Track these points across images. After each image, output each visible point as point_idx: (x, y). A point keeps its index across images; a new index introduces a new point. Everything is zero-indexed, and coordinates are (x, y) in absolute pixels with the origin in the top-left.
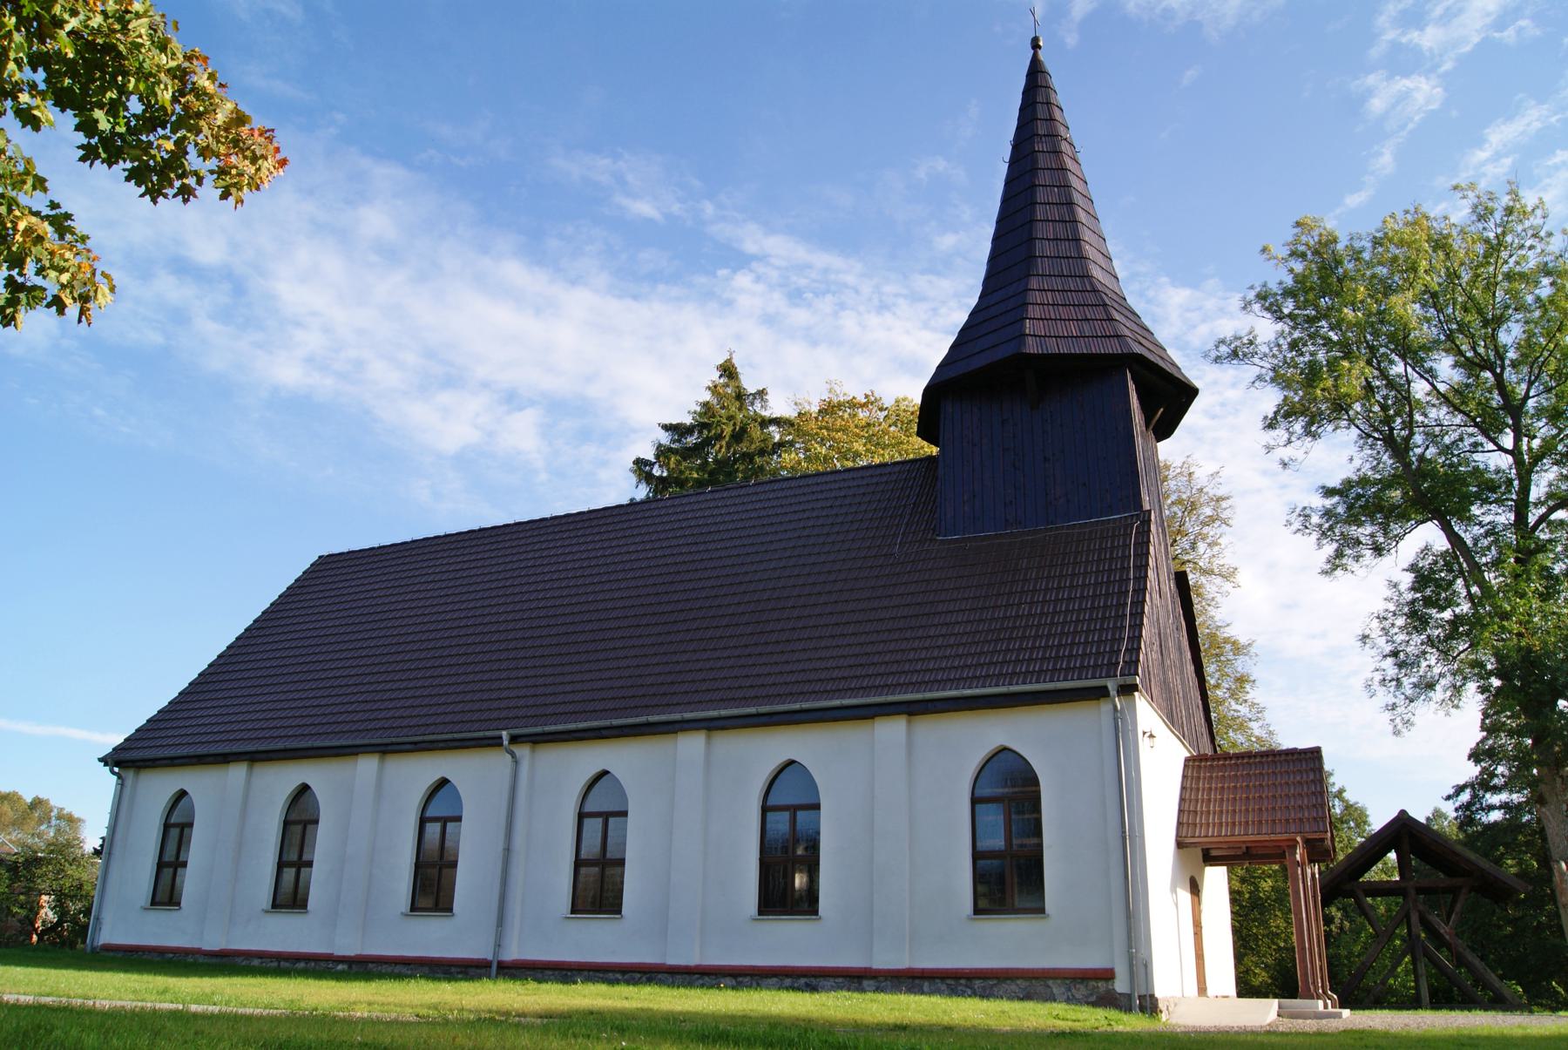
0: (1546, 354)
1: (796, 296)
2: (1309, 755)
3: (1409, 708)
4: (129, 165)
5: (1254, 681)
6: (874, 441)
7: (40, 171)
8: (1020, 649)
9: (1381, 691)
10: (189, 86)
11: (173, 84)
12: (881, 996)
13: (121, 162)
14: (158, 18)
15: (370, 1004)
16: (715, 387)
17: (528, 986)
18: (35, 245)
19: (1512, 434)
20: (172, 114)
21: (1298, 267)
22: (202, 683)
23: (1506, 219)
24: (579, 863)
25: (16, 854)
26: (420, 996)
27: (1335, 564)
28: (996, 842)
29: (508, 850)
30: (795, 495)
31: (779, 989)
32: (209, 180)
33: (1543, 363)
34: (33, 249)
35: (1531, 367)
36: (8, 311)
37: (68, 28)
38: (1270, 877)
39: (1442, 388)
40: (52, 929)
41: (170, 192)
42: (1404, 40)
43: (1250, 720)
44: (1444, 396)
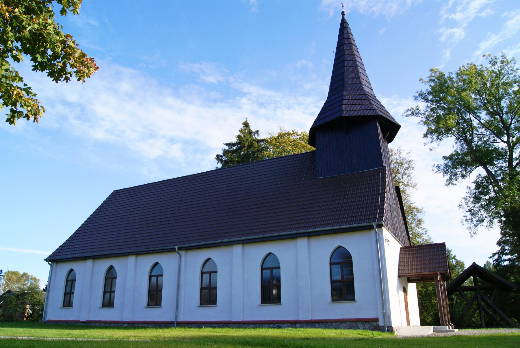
0: (517, 109)
1: (261, 105)
2: (441, 245)
3: (475, 228)
4: (48, 71)
5: (424, 221)
6: (296, 146)
7: (21, 75)
8: (344, 214)
9: (466, 223)
10: (67, 45)
11: (61, 46)
12: (302, 329)
13: (46, 70)
14: (56, 25)
15: (135, 336)
16: (241, 130)
17: (186, 329)
18: (20, 99)
19: (506, 136)
20: (61, 55)
21: (433, 84)
22: (77, 234)
23: (501, 65)
24: (202, 289)
25: (18, 291)
26: (151, 334)
27: (450, 182)
28: (338, 277)
29: (178, 285)
30: (269, 165)
31: (269, 328)
32: (74, 75)
33: (516, 112)
34: (19, 100)
35: (512, 114)
36: (12, 120)
37: (28, 30)
38: (431, 286)
39: (483, 122)
40: (31, 316)
41: (62, 79)
42: (450, 17)
43: (423, 234)
44: (483, 124)
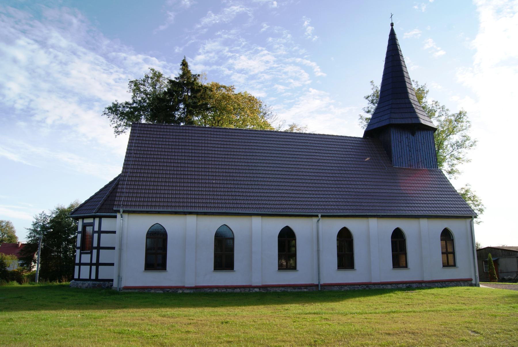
29: (318, 251)
